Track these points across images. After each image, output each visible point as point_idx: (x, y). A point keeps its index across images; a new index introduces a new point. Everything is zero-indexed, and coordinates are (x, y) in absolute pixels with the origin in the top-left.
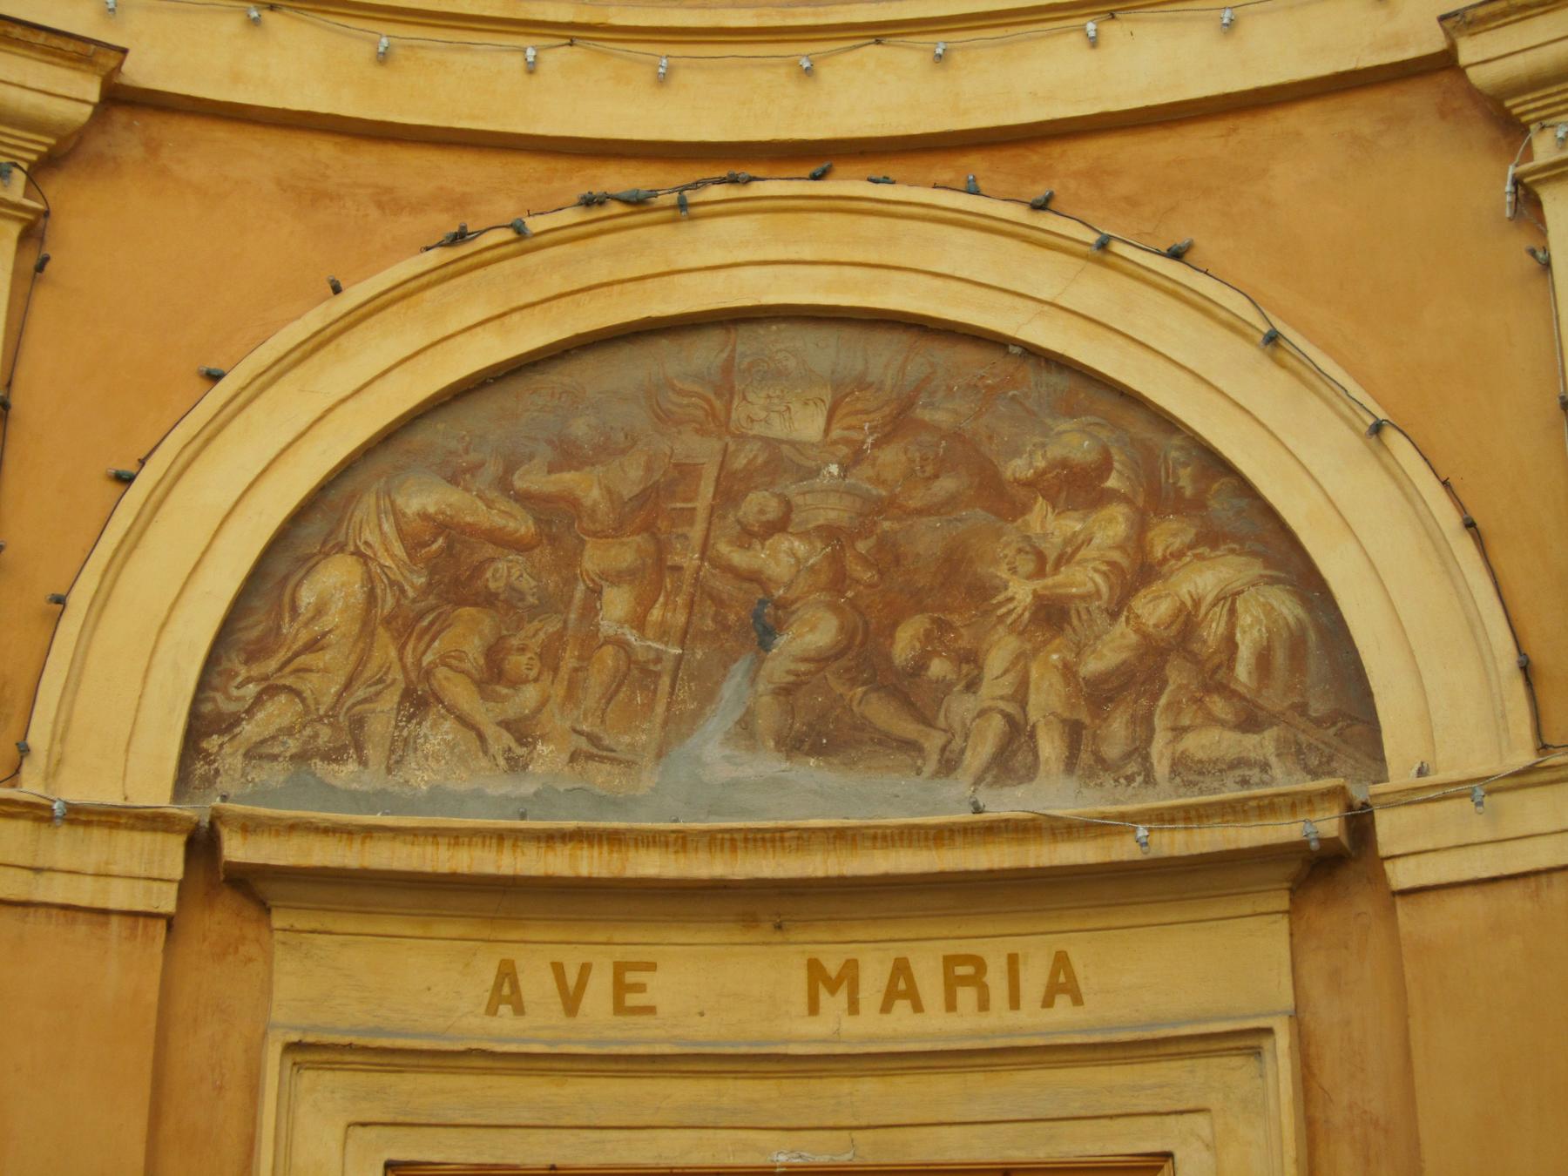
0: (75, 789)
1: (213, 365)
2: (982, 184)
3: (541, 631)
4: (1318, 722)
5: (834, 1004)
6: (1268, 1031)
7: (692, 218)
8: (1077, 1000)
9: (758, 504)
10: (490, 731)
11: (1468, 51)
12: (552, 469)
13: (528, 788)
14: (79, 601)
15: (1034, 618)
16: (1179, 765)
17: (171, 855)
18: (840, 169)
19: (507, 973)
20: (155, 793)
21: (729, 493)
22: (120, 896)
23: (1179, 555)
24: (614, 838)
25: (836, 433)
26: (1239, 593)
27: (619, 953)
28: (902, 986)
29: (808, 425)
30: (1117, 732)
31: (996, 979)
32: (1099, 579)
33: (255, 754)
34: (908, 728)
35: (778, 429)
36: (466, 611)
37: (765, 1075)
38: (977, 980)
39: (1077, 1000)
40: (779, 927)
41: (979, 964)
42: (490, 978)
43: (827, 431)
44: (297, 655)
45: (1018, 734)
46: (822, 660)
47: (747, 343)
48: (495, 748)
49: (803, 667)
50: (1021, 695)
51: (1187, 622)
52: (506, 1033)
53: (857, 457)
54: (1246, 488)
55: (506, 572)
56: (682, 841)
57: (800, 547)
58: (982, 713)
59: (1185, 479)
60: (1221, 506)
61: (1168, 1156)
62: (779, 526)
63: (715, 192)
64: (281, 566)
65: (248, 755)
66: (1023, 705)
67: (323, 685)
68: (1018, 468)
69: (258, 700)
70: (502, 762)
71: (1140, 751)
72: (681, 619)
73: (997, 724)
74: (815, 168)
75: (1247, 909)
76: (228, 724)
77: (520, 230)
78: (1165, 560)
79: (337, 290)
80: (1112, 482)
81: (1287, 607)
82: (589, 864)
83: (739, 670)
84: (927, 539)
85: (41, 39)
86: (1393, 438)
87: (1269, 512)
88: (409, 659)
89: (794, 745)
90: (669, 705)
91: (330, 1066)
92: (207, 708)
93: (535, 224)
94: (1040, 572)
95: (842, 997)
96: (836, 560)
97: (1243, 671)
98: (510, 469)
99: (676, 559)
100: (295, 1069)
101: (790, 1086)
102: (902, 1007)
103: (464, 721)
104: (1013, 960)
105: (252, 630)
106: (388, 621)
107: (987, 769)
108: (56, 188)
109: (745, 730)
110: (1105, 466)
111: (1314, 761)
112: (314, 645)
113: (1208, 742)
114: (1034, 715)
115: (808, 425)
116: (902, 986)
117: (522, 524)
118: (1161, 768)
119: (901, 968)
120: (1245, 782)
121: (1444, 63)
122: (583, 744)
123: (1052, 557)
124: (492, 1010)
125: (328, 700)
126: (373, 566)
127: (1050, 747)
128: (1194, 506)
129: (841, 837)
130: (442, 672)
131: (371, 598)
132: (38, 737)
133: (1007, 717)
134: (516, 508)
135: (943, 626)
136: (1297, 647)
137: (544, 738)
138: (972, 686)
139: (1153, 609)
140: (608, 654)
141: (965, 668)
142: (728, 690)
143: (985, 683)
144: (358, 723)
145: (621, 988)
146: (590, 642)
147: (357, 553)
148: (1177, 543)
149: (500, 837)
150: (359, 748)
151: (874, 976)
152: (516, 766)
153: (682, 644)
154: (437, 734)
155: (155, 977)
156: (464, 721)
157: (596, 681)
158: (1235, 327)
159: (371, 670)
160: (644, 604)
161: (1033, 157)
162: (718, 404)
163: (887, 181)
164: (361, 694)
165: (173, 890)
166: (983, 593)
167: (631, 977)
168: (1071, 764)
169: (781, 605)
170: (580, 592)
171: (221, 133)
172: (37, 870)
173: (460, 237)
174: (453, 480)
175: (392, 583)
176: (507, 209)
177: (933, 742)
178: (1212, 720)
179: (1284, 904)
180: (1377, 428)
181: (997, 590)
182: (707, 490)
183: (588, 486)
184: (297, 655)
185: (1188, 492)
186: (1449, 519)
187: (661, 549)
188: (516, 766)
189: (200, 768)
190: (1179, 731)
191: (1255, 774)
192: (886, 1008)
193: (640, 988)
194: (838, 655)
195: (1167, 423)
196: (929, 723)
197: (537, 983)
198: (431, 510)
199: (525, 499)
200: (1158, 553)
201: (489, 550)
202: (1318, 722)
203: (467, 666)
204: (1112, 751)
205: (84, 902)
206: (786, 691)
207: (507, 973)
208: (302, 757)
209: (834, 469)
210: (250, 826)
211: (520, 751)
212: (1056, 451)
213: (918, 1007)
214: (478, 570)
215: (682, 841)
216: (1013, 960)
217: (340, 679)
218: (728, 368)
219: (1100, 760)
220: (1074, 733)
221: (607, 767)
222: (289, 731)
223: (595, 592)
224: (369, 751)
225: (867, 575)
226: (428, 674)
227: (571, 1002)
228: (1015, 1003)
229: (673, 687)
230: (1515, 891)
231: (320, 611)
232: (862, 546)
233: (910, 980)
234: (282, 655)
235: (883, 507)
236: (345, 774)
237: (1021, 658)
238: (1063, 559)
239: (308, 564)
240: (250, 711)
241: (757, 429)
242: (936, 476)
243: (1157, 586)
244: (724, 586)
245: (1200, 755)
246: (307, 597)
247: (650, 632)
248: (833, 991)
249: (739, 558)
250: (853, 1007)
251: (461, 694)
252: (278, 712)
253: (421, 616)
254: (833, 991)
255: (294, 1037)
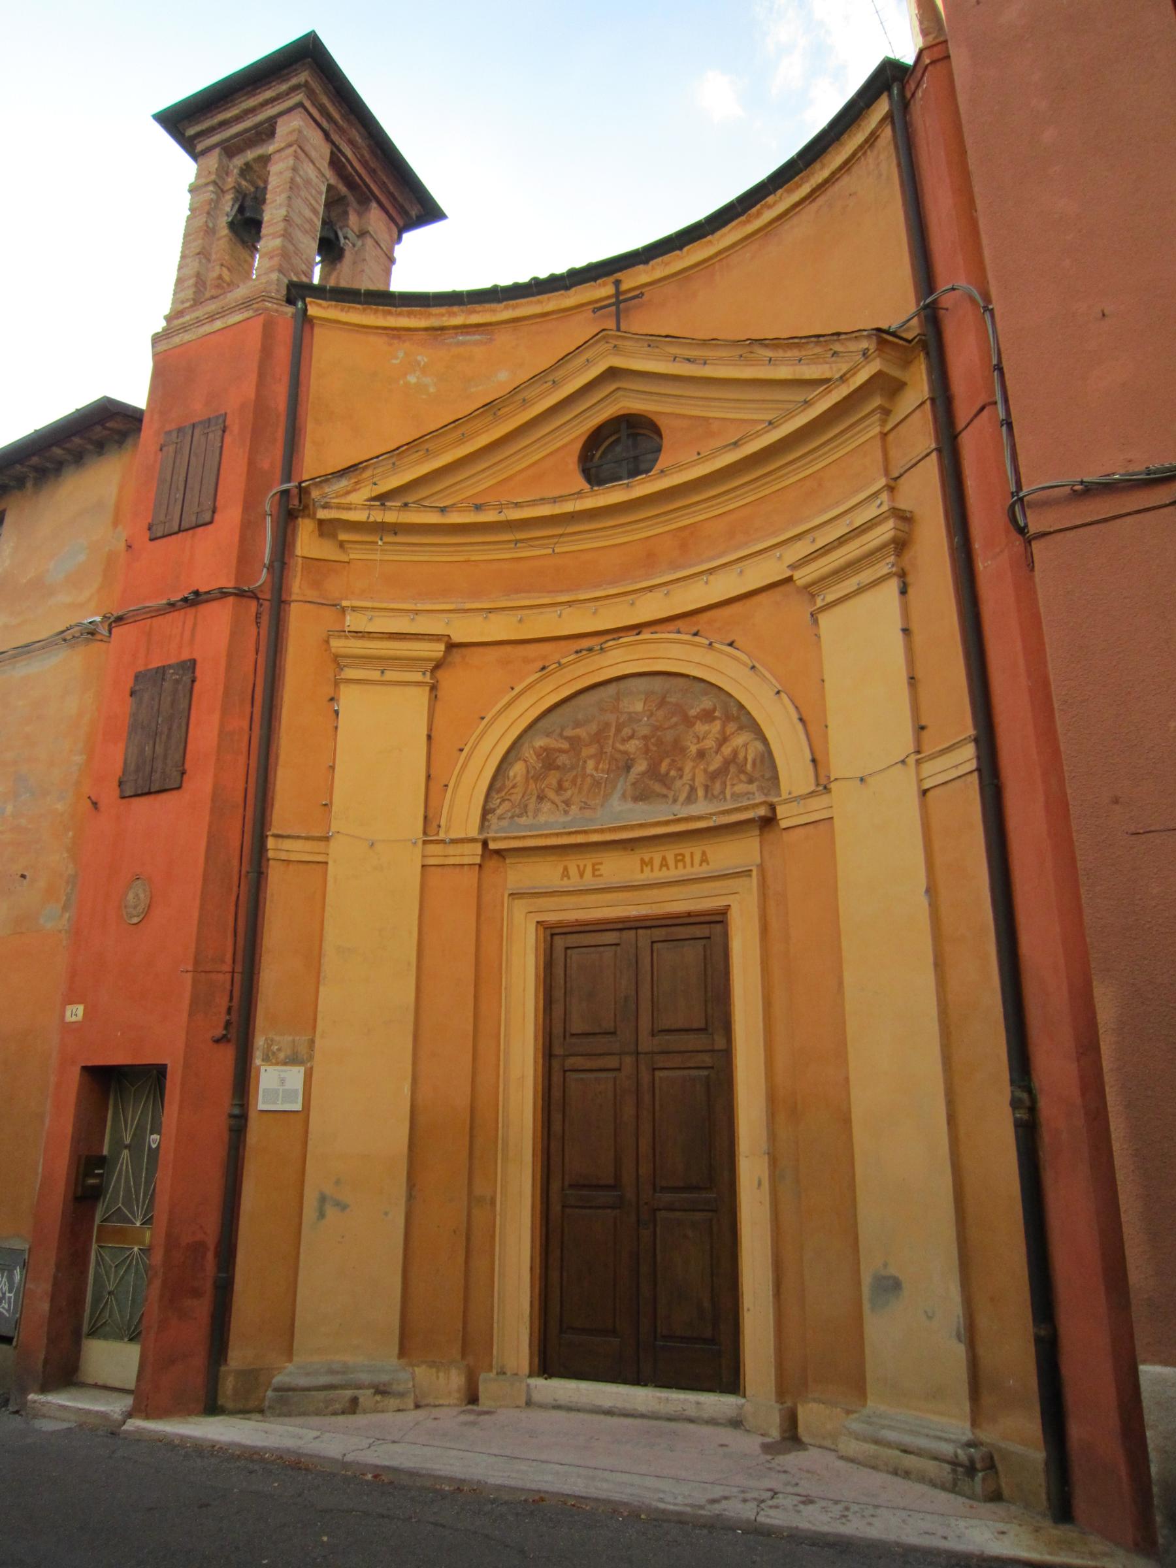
0: (454, 835)
1: (483, 715)
2: (681, 630)
3: (570, 775)
4: (768, 780)
5: (647, 869)
6: (751, 870)
7: (605, 652)
8: (708, 864)
9: (627, 731)
10: (560, 804)
11: (797, 575)
12: (573, 729)
13: (569, 818)
14: (451, 785)
15: (697, 756)
16: (733, 795)
17: (478, 848)
18: (645, 630)
19: (566, 869)
20: (473, 832)
21: (619, 730)
22: (466, 860)
23: (733, 733)
24: (585, 832)
25: (646, 708)
26: (747, 744)
27: (594, 861)
28: (664, 864)
29: (639, 707)
30: (717, 786)
31: (688, 859)
32: (713, 743)
33: (500, 818)
34: (665, 791)
35: (631, 710)
36: (553, 772)
37: (629, 891)
38: (683, 860)
39: (708, 864)
40: (632, 850)
41: (683, 855)
42: (561, 871)
43: (644, 707)
44: (509, 790)
45: (693, 789)
46: (643, 774)
47: (623, 685)
48: (561, 808)
49: (638, 777)
50: (693, 779)
51: (735, 753)
52: (566, 884)
53: (652, 714)
54: (749, 713)
55: (562, 759)
56: (602, 831)
57: (637, 742)
58: (683, 785)
59: (735, 711)
60: (744, 719)
61: (729, 906)
62: (631, 737)
63: (611, 643)
64: (504, 766)
65: (499, 819)
66: (694, 783)
67: (516, 797)
68: (692, 712)
69: (500, 803)
70: (562, 812)
71: (723, 792)
72: (607, 767)
73: (687, 787)
74: (637, 631)
75: (749, 835)
76: (493, 811)
77: (559, 663)
78: (729, 736)
79: (512, 689)
80: (717, 714)
81: (759, 746)
82: (580, 839)
83: (622, 779)
84: (669, 736)
85: (427, 637)
86: (783, 695)
87: (754, 719)
88: (538, 787)
89: (637, 799)
90: (604, 791)
91: (520, 898)
92: (487, 807)
93: (563, 661)
94: (698, 742)
95: (649, 867)
96: (646, 745)
97: (749, 767)
98: (562, 730)
99: (605, 750)
100: (511, 898)
101: (636, 893)
102: (664, 869)
103: (553, 803)
104: (692, 854)
105: (498, 785)
106: (532, 777)
107: (685, 800)
108: (440, 674)
109: (624, 796)
110: (714, 710)
111: (765, 791)
112: (514, 787)
113: (741, 788)
114: (697, 784)
115: (639, 707)
116: (664, 864)
117: (565, 745)
118: (728, 796)
119: (664, 858)
120: (749, 799)
121: (789, 579)
122: (583, 805)
123: (701, 737)
124: (562, 879)
125: (518, 801)
126: (528, 763)
127: (701, 793)
128: (737, 719)
129: (641, 826)
130: (547, 789)
131: (528, 772)
132: (443, 823)
133: (691, 786)
134: (563, 741)
135: (673, 761)
136: (762, 757)
137: (573, 804)
138: (681, 777)
139: (727, 750)
140: (589, 780)
141: (679, 772)
142: (619, 786)
143: (684, 776)
144: (526, 806)
145: (594, 870)
146: (584, 776)
147: (524, 760)
148: (733, 730)
149: (557, 835)
150: (526, 813)
151: (657, 862)
152: (566, 813)
153: (608, 774)
154: (546, 806)
155: (476, 880)
156: (553, 803)
157: (586, 787)
158: (745, 664)
159: (529, 792)
160: (598, 763)
161: (694, 619)
162: (616, 704)
163: (656, 633)
164: (526, 798)
165: (479, 857)
166: (683, 750)
167: (597, 867)
168: (706, 796)
169: (632, 760)
170: (581, 763)
171: (481, 650)
172: (446, 856)
173: (544, 668)
174: (547, 736)
175: (534, 767)
176: (556, 657)
177: (671, 795)
178: (741, 781)
179: (757, 832)
180: (778, 692)
181: (688, 749)
182: (613, 730)
183: (582, 732)
184: (509, 790)
185: (735, 715)
186: (795, 716)
187: (602, 747)
188: (566, 813)
189: (486, 823)
190: (733, 785)
191: (751, 796)
192: (660, 870)
193: (599, 870)
194: (648, 771)
195: (730, 696)
196: (669, 788)
197: (573, 871)
198: (542, 745)
199: (566, 738)
200: (728, 733)
201: (558, 754)
202: (768, 780)
203: (553, 787)
204: (716, 793)
205: (457, 863)
206: (634, 784)
207: (566, 869)
208: (512, 817)
209: (646, 719)
210: (495, 839)
211: (567, 808)
212: (702, 706)
213: (668, 869)
214: (554, 760)
215: (602, 831)
216: (692, 854)
217: (521, 795)
218: (618, 693)
219: (713, 795)
220: (707, 788)
221: (588, 810)
222: (508, 811)
223: (585, 762)
224: (529, 813)
225: (654, 749)
226: (543, 791)
227: (582, 875)
228: (692, 865)
229: (605, 787)
230: (811, 826)
231: (515, 777)
232: (653, 740)
233: (666, 862)
234: (506, 790)
235: (657, 728)
236: (523, 820)
237: (694, 768)
238: (704, 738)
239: (511, 764)
240: (498, 807)
241: (626, 710)
242: (671, 718)
243: (728, 744)
244: (618, 756)
245: (738, 792)
246: (511, 774)
247: (599, 771)
248: (647, 866)
249: (622, 748)
250: (652, 870)
251: (551, 795)
252: (506, 805)
253: (541, 775)
254: (647, 866)
255: (511, 892)
